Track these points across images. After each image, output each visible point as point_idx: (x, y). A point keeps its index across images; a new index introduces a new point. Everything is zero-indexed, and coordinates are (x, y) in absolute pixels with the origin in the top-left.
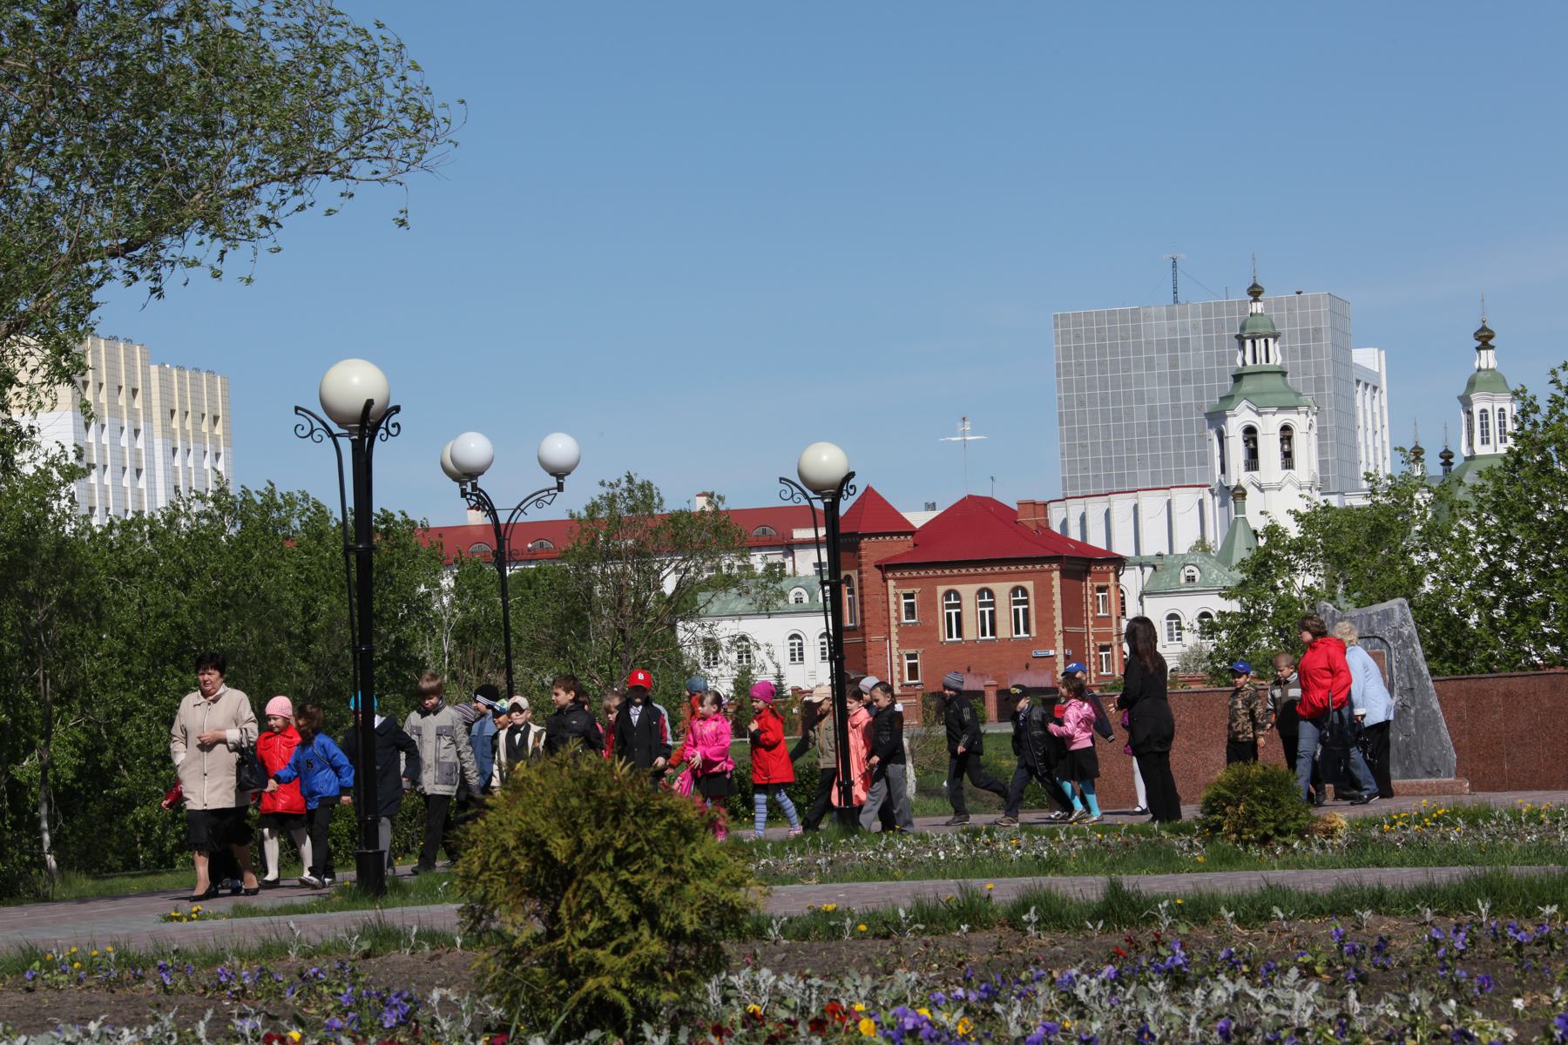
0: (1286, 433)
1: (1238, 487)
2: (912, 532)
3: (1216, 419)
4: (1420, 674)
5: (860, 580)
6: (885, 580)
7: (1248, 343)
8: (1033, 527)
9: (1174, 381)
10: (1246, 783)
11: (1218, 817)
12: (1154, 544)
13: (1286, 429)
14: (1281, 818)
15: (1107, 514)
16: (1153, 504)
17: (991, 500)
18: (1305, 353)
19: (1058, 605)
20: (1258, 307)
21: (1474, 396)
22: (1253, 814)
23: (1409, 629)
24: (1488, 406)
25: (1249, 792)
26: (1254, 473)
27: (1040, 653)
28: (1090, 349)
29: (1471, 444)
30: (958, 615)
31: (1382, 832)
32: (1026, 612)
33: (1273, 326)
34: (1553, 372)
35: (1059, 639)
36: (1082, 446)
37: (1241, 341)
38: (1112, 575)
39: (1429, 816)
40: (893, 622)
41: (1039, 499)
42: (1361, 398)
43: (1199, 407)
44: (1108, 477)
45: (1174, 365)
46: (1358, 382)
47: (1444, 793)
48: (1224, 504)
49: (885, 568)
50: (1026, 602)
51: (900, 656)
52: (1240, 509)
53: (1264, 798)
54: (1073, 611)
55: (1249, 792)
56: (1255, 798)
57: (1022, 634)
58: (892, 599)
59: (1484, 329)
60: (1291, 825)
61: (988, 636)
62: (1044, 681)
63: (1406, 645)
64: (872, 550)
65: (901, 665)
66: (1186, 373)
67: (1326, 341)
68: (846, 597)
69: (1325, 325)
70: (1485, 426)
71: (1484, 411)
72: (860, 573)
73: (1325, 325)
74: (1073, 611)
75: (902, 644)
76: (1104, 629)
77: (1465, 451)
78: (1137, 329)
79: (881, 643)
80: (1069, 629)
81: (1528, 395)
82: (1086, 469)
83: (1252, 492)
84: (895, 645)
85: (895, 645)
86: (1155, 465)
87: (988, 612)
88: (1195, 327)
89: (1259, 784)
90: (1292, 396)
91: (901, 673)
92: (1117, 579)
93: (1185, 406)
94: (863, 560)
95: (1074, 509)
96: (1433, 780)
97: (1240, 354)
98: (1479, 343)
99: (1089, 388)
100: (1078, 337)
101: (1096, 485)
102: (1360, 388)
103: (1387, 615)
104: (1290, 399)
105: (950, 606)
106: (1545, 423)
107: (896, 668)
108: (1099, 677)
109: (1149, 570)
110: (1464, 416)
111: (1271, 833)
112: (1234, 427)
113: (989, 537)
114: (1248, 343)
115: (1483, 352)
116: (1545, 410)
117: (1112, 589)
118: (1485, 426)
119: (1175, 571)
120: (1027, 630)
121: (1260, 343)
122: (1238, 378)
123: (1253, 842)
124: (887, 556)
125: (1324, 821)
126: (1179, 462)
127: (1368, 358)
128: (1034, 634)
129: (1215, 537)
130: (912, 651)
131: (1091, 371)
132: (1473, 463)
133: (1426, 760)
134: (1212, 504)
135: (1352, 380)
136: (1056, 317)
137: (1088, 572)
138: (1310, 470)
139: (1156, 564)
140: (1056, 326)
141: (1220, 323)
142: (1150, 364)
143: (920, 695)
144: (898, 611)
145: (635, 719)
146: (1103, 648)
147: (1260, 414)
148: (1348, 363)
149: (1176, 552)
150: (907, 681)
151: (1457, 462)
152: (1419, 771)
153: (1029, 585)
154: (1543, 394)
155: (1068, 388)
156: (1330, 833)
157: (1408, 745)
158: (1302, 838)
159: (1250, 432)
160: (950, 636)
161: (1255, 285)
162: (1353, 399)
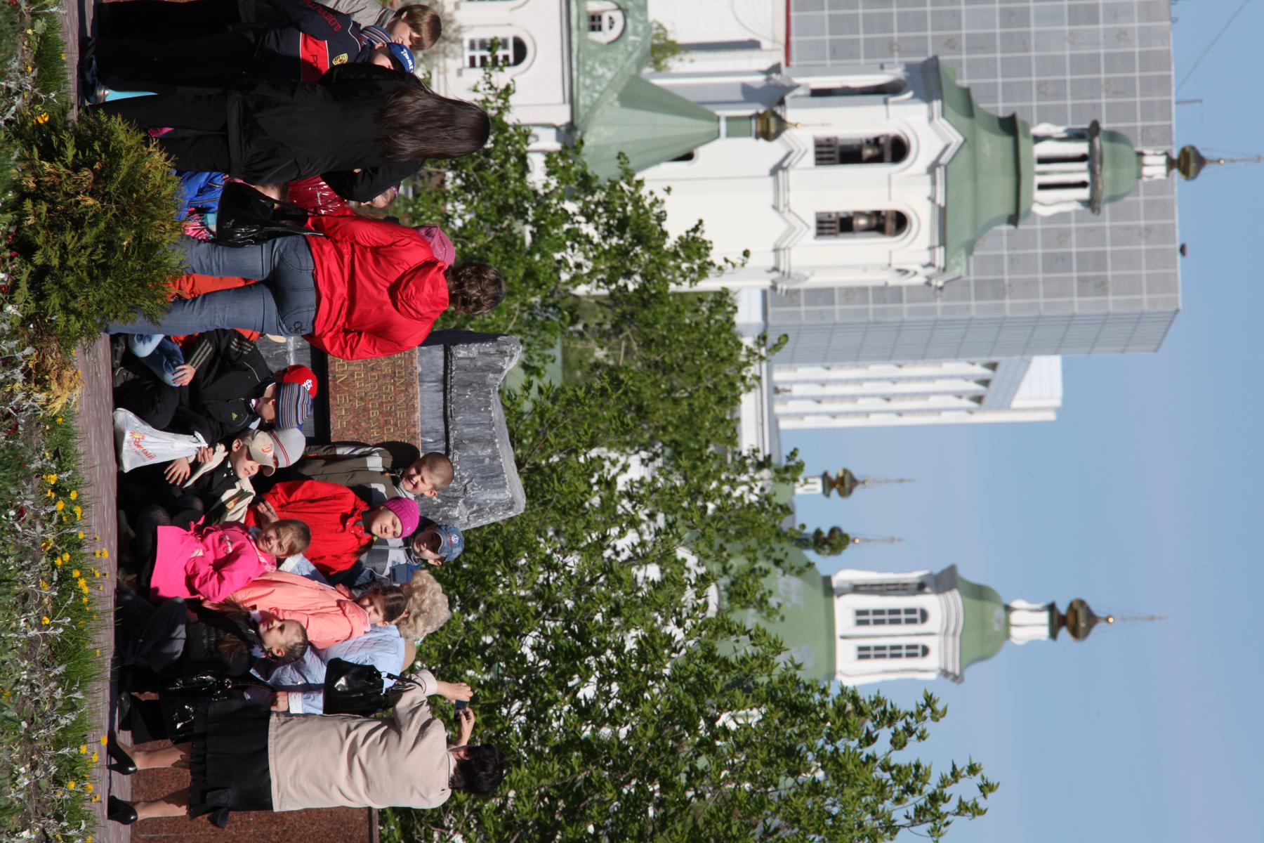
0: (891, 223)
1: (782, 124)
3: (926, 81)
7: (1081, 148)
10: (142, 212)
11: (70, 153)
13: (901, 221)
14: (69, 280)
18: (1057, 262)
20: (1155, 167)
21: (954, 597)
22: (78, 224)
24: (934, 623)
25: (122, 217)
26: (810, 157)
29: (857, 589)
31: (41, 472)
33: (1113, 199)
34: (973, 770)
37: (1089, 133)
42: (960, 372)
43: (952, 44)
46: (993, 366)
48: (749, 93)
52: (736, 127)
53: (110, 247)
55: (122, 217)
56: (110, 229)
59: (1092, 619)
60: (55, 300)
67: (1079, 304)
69: (1112, 302)
70: (894, 617)
71: (924, 616)
73: (1112, 302)
77: (842, 577)
81: (929, 725)
83: (772, 151)
88: (1122, 36)
89: (138, 238)
90: (967, 236)
93: (956, 15)
97: (1059, 131)
98: (1063, 609)
103: (491, 476)
104: (961, 230)
106: (871, 759)
110: (914, 576)
111: (38, 259)
112: (906, 117)
114: (1081, 148)
115: (1044, 617)
116: (901, 758)
118: (894, 617)
121: (1079, 172)
122: (1009, 126)
123: (18, 223)
125: (64, 365)
127: (1041, 386)
129: (681, 74)
132: (819, 591)
134: (749, 68)
135: (996, 355)
138: (813, 270)
141: (1126, 87)
147: (932, 169)
148: (1030, 348)
151: (822, 562)
154: (933, 752)
156: (38, 377)
158: (25, 322)
159: (896, 150)
161: (1201, 161)
162: (957, 356)
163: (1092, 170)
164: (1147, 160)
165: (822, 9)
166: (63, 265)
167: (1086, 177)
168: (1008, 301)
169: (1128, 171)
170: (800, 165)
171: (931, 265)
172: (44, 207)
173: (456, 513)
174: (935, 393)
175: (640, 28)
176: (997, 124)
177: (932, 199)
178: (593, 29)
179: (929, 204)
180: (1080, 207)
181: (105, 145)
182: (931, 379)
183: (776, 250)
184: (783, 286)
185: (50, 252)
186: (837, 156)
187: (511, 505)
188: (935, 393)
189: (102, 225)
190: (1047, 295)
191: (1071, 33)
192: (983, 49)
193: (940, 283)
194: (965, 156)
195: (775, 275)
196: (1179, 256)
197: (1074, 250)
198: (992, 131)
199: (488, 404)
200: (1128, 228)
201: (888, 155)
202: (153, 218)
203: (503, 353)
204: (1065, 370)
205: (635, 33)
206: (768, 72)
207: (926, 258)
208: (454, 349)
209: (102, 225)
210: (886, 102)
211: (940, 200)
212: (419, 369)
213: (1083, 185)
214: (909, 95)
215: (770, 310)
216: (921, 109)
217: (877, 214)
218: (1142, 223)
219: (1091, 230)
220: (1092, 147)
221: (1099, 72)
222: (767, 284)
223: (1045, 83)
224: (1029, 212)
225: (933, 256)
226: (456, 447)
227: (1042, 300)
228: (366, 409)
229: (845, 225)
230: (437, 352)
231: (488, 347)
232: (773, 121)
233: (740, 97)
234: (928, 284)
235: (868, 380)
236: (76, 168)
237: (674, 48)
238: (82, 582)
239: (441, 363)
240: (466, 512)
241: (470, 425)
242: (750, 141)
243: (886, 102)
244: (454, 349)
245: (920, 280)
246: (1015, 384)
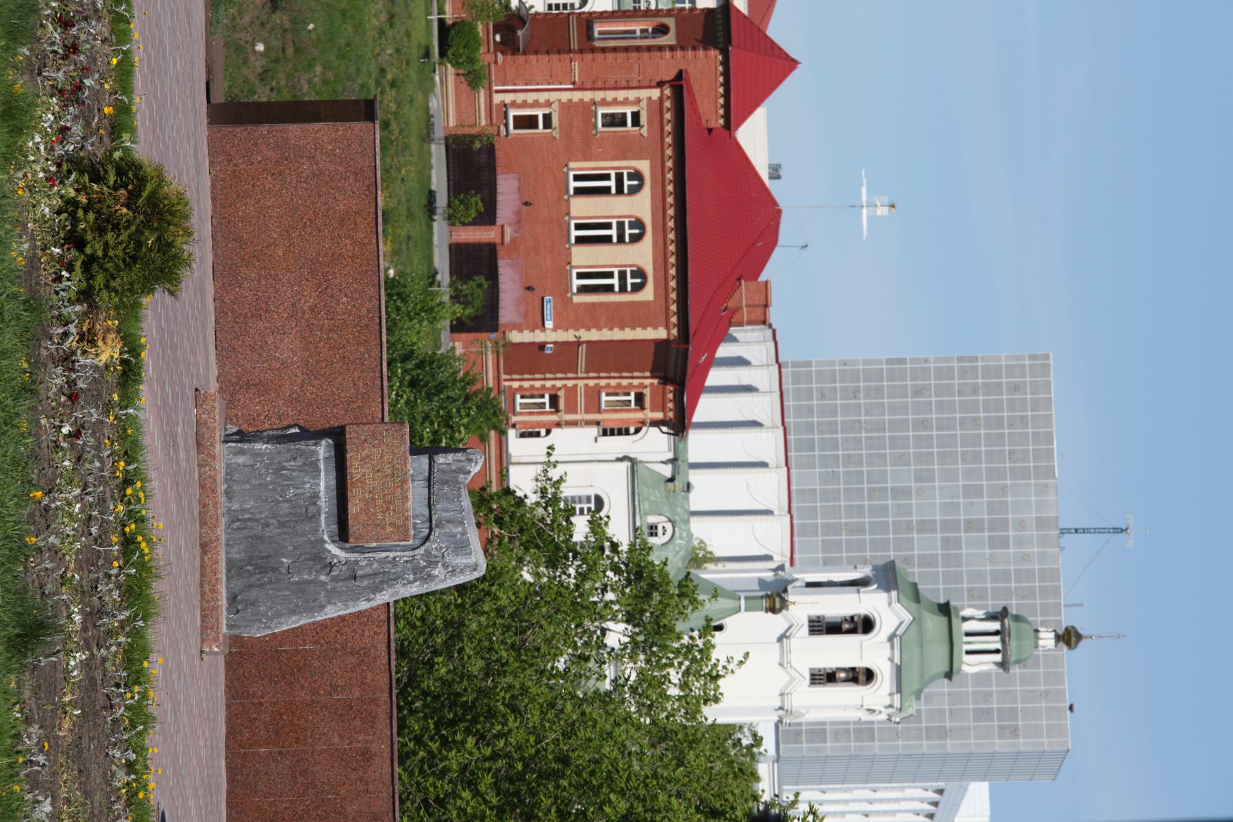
2: (730, 125)
3: (887, 577)
4: (376, 589)
5: (660, 48)
6: (660, 85)
7: (996, 626)
8: (731, 304)
9: (948, 526)
10: (161, 220)
11: (112, 179)
12: (707, 490)
13: (869, 675)
15: (755, 424)
16: (768, 488)
17: (774, 243)
18: (983, 714)
19: (617, 335)
20: (1047, 640)
23: (443, 580)
25: (147, 224)
26: (806, 629)
27: (548, 308)
28: (998, 405)
30: (605, 191)
32: (609, 289)
35: (568, 336)
36: (856, 392)
37: (1000, 615)
38: (659, 415)
39: (139, 531)
40: (598, 96)
41: (774, 314)
44: (809, 428)
45: (970, 526)
46: (940, 792)
47: (204, 617)
49: (679, 85)
50: (623, 289)
51: (548, 104)
53: (139, 244)
54: (609, 358)
55: (147, 224)
56: (139, 231)
57: (576, 283)
58: (632, 94)
60: (100, 280)
61: (575, 233)
62: (508, 311)
63: (417, 570)
64: (704, 67)
65: (536, 104)
66: (957, 544)
68: (637, 27)
69: (1023, 744)
72: (672, 48)
74: (609, 358)
75: (567, 107)
76: (581, 401)
78: (1025, 473)
79: (567, 76)
80: (583, 350)
82: (822, 396)
83: (777, 623)
84: (565, 96)
85: (565, 96)
86: (825, 496)
87: (613, 234)
88: (1026, 558)
89: (158, 239)
90: (916, 687)
91: (524, 105)
92: (655, 423)
93: (911, 541)
94: (690, 53)
95: (764, 377)
96: (223, 602)
97: (980, 613)
100: (1016, 388)
101: (798, 411)
102: (932, 795)
103: (461, 546)
104: (911, 683)
105: (619, 178)
107: (531, 97)
108: (513, 392)
109: (667, 471)
111: (88, 250)
113: (719, 238)
114: (996, 626)
117: (639, 415)
119: (666, 509)
120: (584, 290)
121: (995, 643)
124: (696, 88)
128: (578, 299)
130: (555, 121)
131: (965, 407)
133: (253, 594)
136: (1047, 357)
137: (665, 380)
139: (676, 480)
140: (1033, 357)
141: (1030, 593)
142: (972, 491)
143: (493, 130)
144: (615, 102)
146: (554, 400)
147: (891, 639)
149: (693, 519)
150: (512, 113)
152: (238, 584)
153: (648, 294)
155: (941, 373)
157: (275, 570)
159: (866, 625)
160: (577, 178)
161: (1079, 637)
163: (1003, 641)
164: (1041, 635)
165: (817, 535)
166: (105, 256)
167: (999, 646)
168: (949, 742)
169: (1028, 643)
170: (799, 634)
171: (891, 706)
172: (91, 216)
173: (436, 572)
174: (900, 811)
175: (685, 534)
176: (936, 608)
177: (891, 660)
178: (652, 535)
179: (889, 663)
180: (994, 667)
181: (136, 175)
182: (897, 800)
183: (782, 695)
184: (787, 720)
185: (97, 246)
186: (824, 628)
187: (475, 568)
188: (900, 811)
189: (133, 228)
190: (976, 738)
191: (991, 555)
192: (929, 565)
193: (898, 720)
194: (914, 628)
195: (781, 713)
196: (1068, 712)
197: (995, 706)
198: (933, 613)
199: (459, 496)
200: (1032, 691)
201: (860, 628)
202: (169, 224)
203: (470, 460)
204: (992, 796)
205: (681, 538)
206: (775, 570)
207: (888, 702)
208: (436, 458)
209: (133, 228)
210: (858, 592)
211: (897, 660)
212: (411, 472)
213: (997, 651)
214: (875, 586)
215: (781, 746)
216: (882, 597)
217: (853, 669)
218: (1042, 688)
219: (1007, 692)
220: (1003, 625)
221: (1010, 582)
222: (777, 719)
223: (973, 589)
224: (959, 670)
225: (893, 700)
226: (437, 526)
227: (973, 741)
228: (373, 499)
229: (830, 677)
230: (424, 460)
231: (460, 456)
232: (777, 600)
233: (757, 587)
234: (889, 720)
235: (853, 801)
236: (116, 189)
237: (711, 559)
238: (143, 545)
239: (427, 467)
240: (444, 572)
241: (446, 511)
242: (762, 614)
243: (858, 592)
244: (436, 458)
245: (884, 717)
246: (956, 806)
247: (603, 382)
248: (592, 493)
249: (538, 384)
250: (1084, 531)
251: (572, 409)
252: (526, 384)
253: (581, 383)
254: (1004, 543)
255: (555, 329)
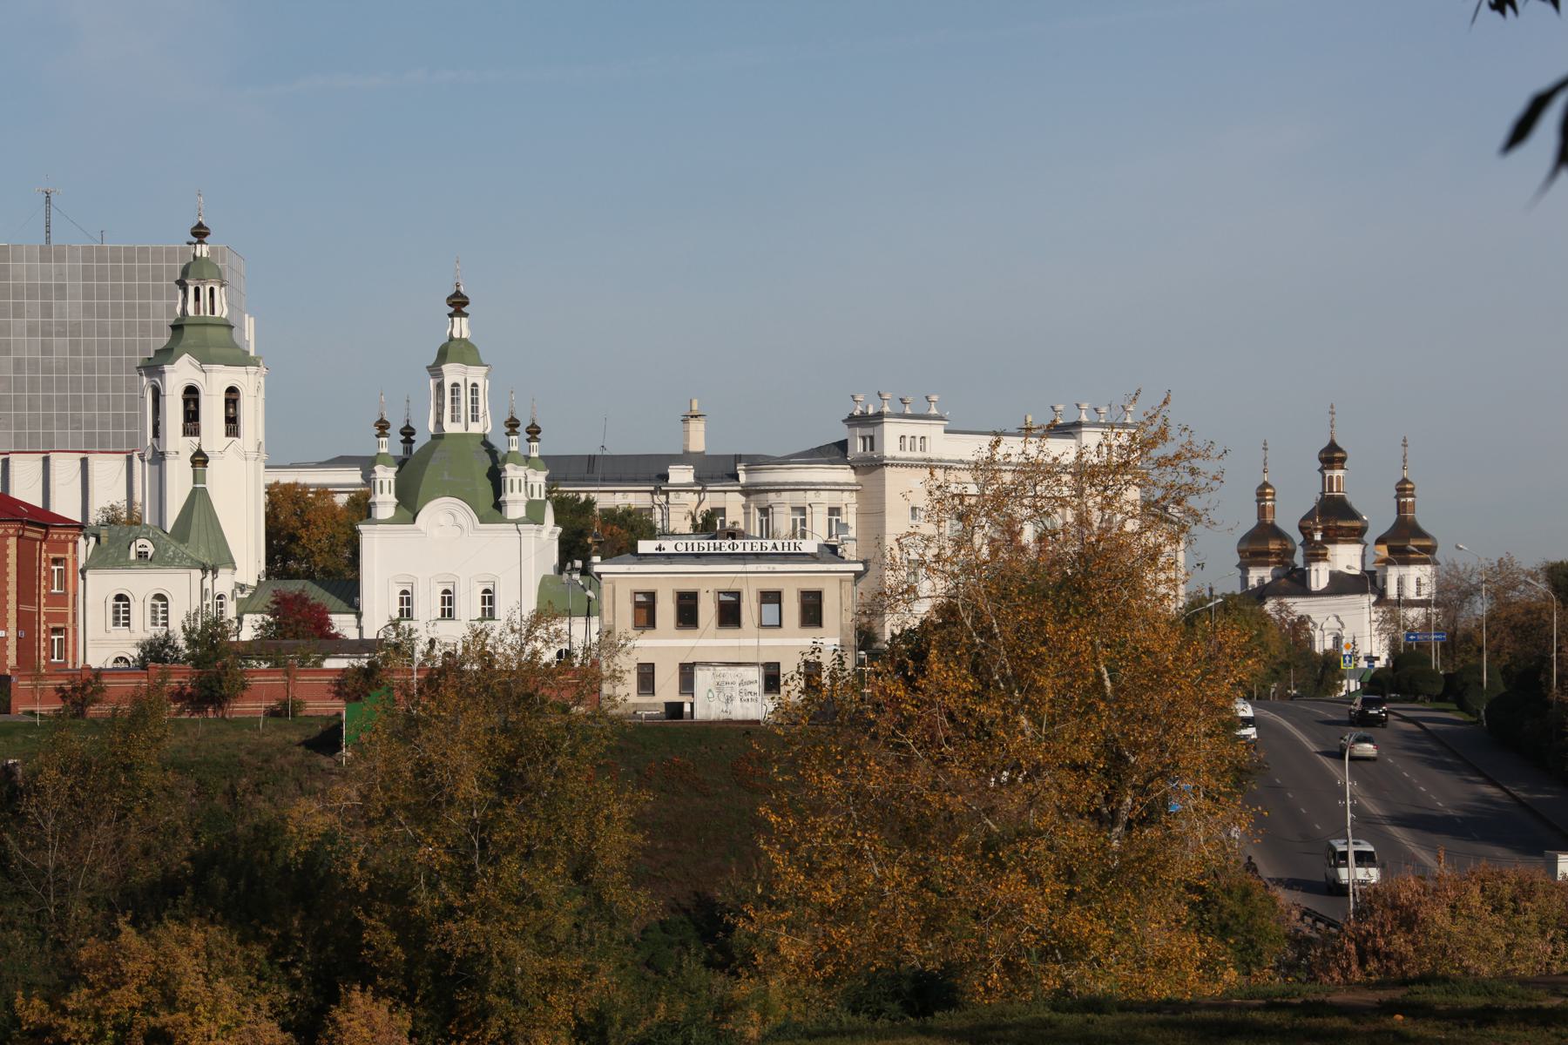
3: (154, 367)
13: (232, 391)
38: (70, 545)
71: (455, 385)
80: (23, 607)
98: (452, 310)
99: (133, 306)
108: (49, 664)
115: (456, 320)
126: (48, 421)
145: (1244, 732)
146: (56, 631)
151: (420, 441)
159: (191, 394)
247: (43, 591)
248: (111, 602)
249: (43, 644)
250: (48, 226)
251: (64, 617)
252: (43, 654)
253: (43, 609)
254: (61, 288)
255: (6, 629)
